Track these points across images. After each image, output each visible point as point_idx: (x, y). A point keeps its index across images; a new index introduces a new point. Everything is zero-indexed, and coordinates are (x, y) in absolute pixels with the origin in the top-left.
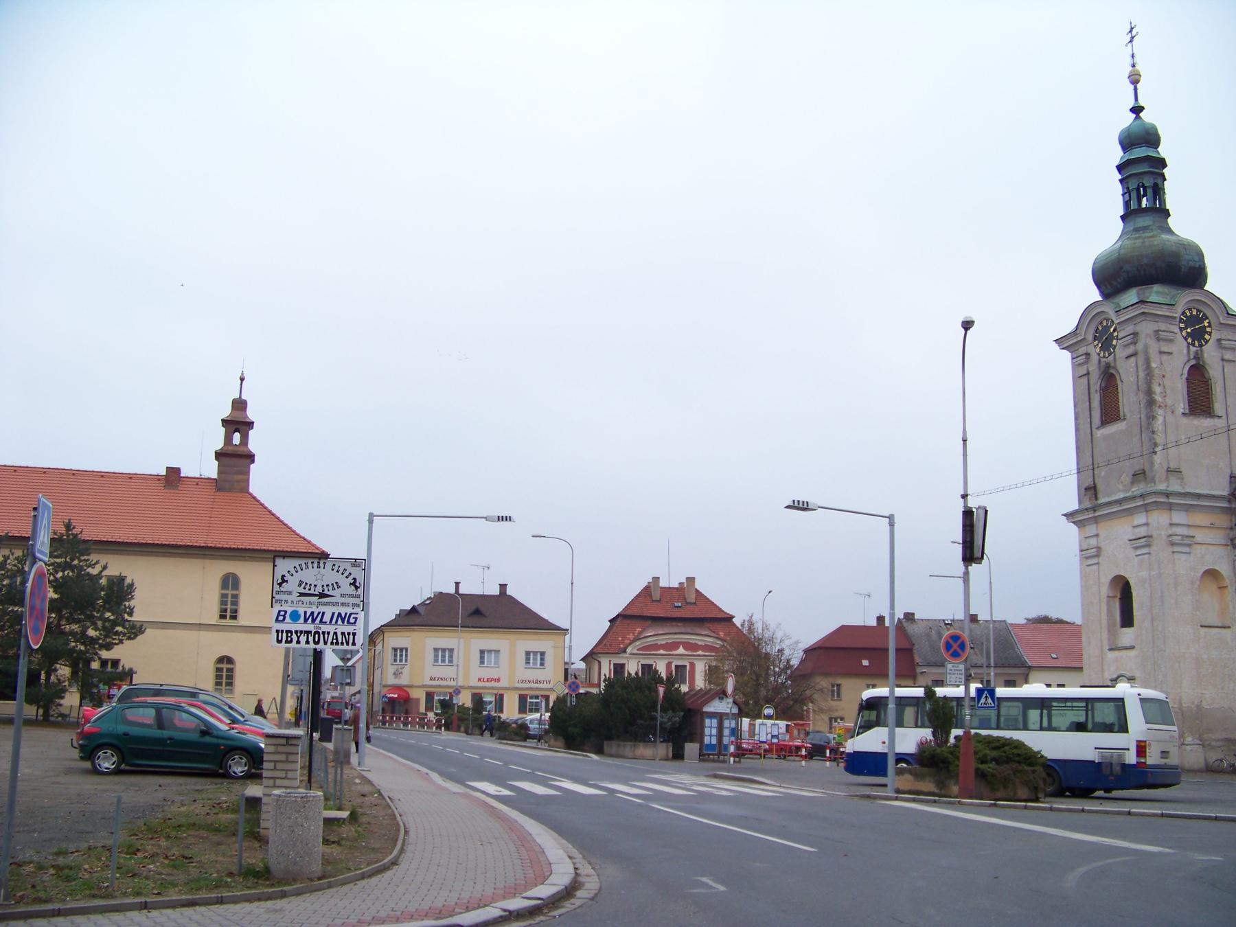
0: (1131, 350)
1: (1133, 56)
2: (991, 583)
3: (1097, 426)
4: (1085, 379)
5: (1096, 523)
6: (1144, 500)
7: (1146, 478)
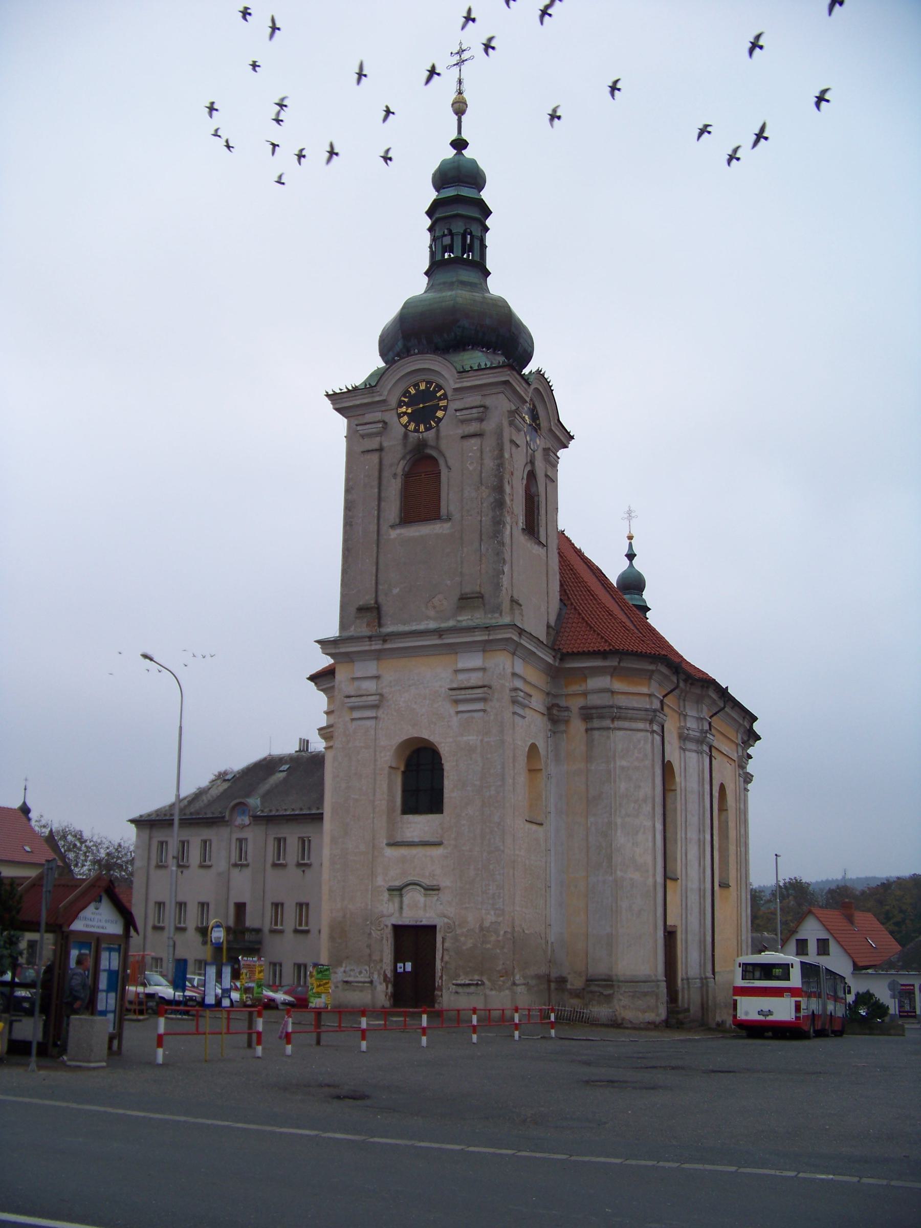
0: (473, 428)
1: (460, 82)
2: (181, 727)
3: (392, 522)
4: (375, 457)
5: (378, 659)
6: (489, 635)
7: (484, 605)
